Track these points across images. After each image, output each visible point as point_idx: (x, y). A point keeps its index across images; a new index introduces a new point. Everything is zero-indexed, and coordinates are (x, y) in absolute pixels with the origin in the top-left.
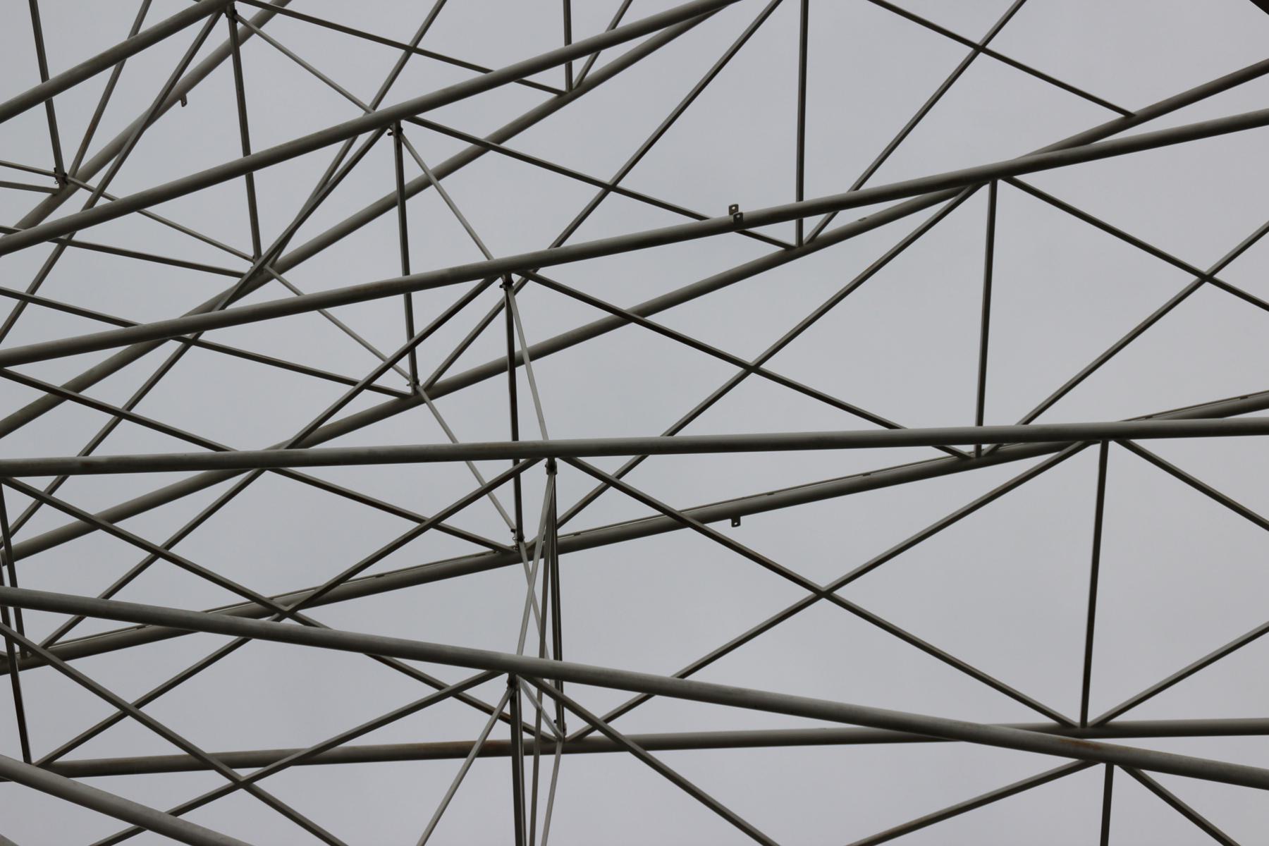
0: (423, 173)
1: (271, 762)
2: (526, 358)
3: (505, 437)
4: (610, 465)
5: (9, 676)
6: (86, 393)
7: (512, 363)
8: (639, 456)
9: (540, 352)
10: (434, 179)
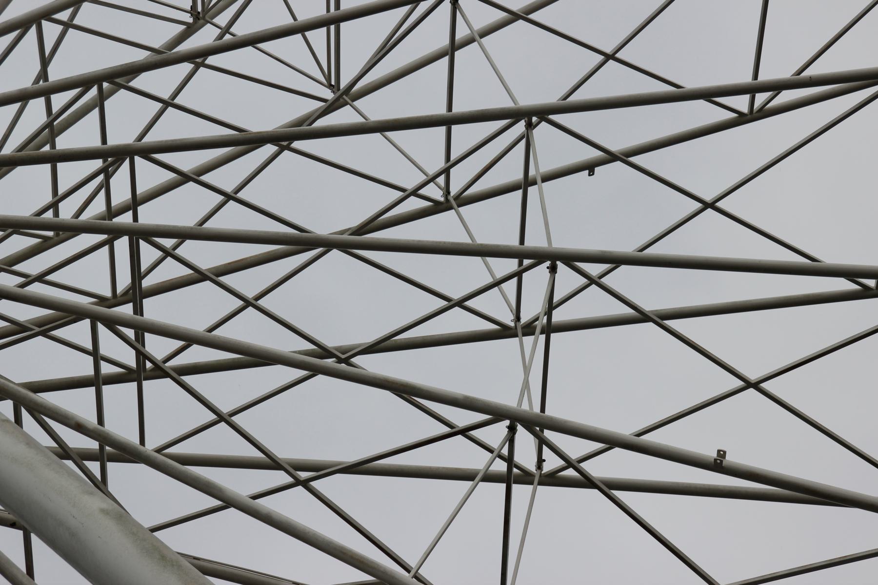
0: (469, 32)
1: (323, 470)
2: (539, 180)
3: (513, 241)
4: (594, 269)
5: (135, 384)
6: (204, 178)
7: (526, 183)
8: (614, 265)
9: (548, 178)
10: (477, 37)
